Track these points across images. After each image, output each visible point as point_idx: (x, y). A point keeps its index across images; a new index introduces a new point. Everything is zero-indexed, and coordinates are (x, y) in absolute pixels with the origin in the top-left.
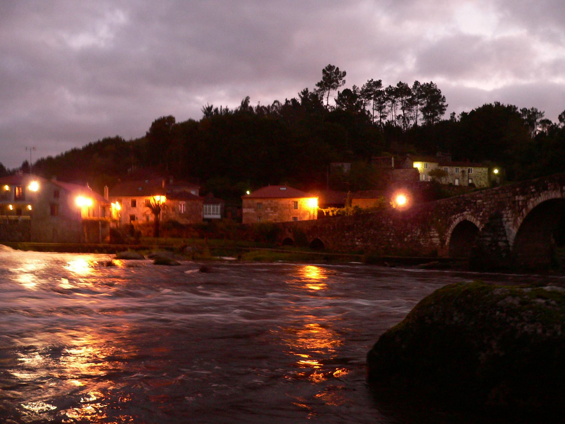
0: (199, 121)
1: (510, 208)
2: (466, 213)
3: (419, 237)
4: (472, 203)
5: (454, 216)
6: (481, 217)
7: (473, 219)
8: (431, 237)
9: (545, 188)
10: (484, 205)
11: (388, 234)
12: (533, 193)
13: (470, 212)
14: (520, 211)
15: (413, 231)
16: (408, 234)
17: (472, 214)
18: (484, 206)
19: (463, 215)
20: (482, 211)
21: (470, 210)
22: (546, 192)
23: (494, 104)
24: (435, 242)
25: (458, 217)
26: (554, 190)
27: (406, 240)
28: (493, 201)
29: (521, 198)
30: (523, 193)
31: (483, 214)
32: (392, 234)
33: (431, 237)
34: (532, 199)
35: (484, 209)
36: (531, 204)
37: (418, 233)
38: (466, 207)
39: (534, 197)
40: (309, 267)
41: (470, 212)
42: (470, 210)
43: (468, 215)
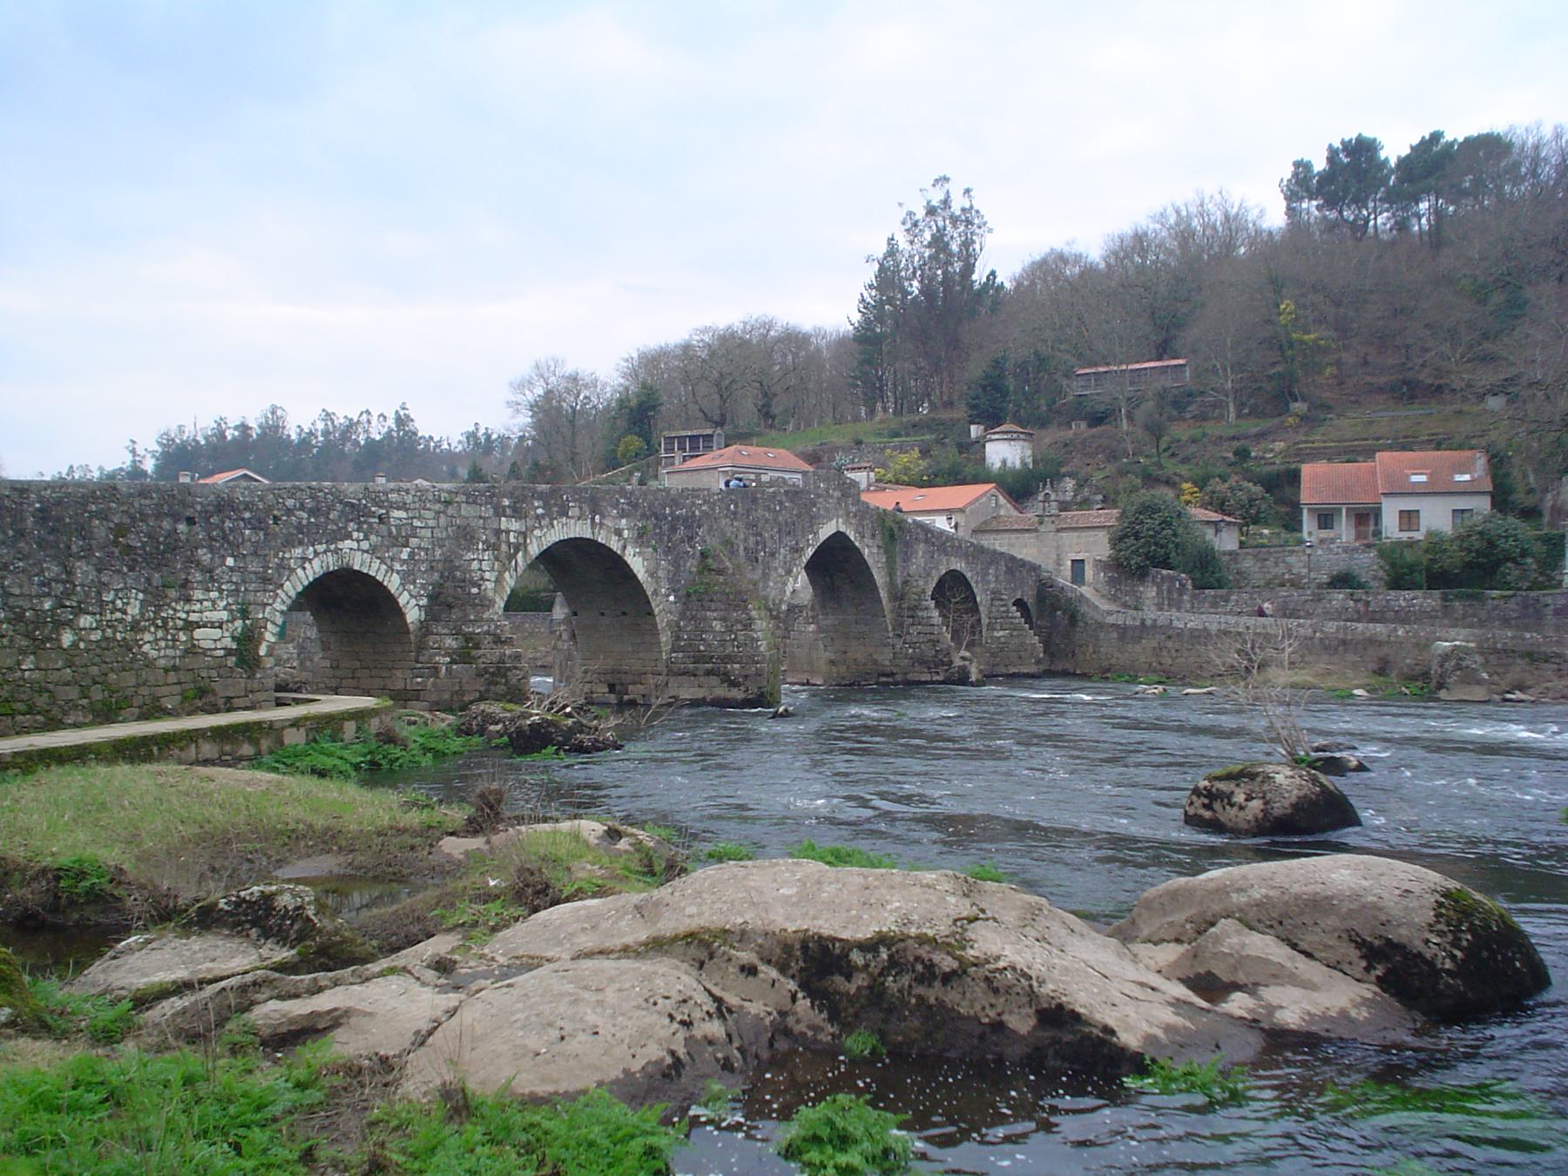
0: (1270, 212)
1: (489, 546)
2: (348, 543)
3: (135, 627)
4: (372, 515)
5: (298, 551)
8: (190, 626)
9: (564, 512)
12: (538, 517)
13: (365, 545)
14: (512, 557)
15: (108, 597)
16: (79, 611)
19: (337, 551)
21: (366, 538)
23: (998, 465)
24: (205, 644)
27: (67, 638)
28: (443, 520)
29: (515, 525)
30: (517, 513)
31: (412, 555)
33: (190, 626)
34: (537, 532)
35: (414, 541)
37: (134, 610)
38: (352, 526)
39: (541, 528)
41: (365, 545)
42: (366, 538)
43: (357, 554)
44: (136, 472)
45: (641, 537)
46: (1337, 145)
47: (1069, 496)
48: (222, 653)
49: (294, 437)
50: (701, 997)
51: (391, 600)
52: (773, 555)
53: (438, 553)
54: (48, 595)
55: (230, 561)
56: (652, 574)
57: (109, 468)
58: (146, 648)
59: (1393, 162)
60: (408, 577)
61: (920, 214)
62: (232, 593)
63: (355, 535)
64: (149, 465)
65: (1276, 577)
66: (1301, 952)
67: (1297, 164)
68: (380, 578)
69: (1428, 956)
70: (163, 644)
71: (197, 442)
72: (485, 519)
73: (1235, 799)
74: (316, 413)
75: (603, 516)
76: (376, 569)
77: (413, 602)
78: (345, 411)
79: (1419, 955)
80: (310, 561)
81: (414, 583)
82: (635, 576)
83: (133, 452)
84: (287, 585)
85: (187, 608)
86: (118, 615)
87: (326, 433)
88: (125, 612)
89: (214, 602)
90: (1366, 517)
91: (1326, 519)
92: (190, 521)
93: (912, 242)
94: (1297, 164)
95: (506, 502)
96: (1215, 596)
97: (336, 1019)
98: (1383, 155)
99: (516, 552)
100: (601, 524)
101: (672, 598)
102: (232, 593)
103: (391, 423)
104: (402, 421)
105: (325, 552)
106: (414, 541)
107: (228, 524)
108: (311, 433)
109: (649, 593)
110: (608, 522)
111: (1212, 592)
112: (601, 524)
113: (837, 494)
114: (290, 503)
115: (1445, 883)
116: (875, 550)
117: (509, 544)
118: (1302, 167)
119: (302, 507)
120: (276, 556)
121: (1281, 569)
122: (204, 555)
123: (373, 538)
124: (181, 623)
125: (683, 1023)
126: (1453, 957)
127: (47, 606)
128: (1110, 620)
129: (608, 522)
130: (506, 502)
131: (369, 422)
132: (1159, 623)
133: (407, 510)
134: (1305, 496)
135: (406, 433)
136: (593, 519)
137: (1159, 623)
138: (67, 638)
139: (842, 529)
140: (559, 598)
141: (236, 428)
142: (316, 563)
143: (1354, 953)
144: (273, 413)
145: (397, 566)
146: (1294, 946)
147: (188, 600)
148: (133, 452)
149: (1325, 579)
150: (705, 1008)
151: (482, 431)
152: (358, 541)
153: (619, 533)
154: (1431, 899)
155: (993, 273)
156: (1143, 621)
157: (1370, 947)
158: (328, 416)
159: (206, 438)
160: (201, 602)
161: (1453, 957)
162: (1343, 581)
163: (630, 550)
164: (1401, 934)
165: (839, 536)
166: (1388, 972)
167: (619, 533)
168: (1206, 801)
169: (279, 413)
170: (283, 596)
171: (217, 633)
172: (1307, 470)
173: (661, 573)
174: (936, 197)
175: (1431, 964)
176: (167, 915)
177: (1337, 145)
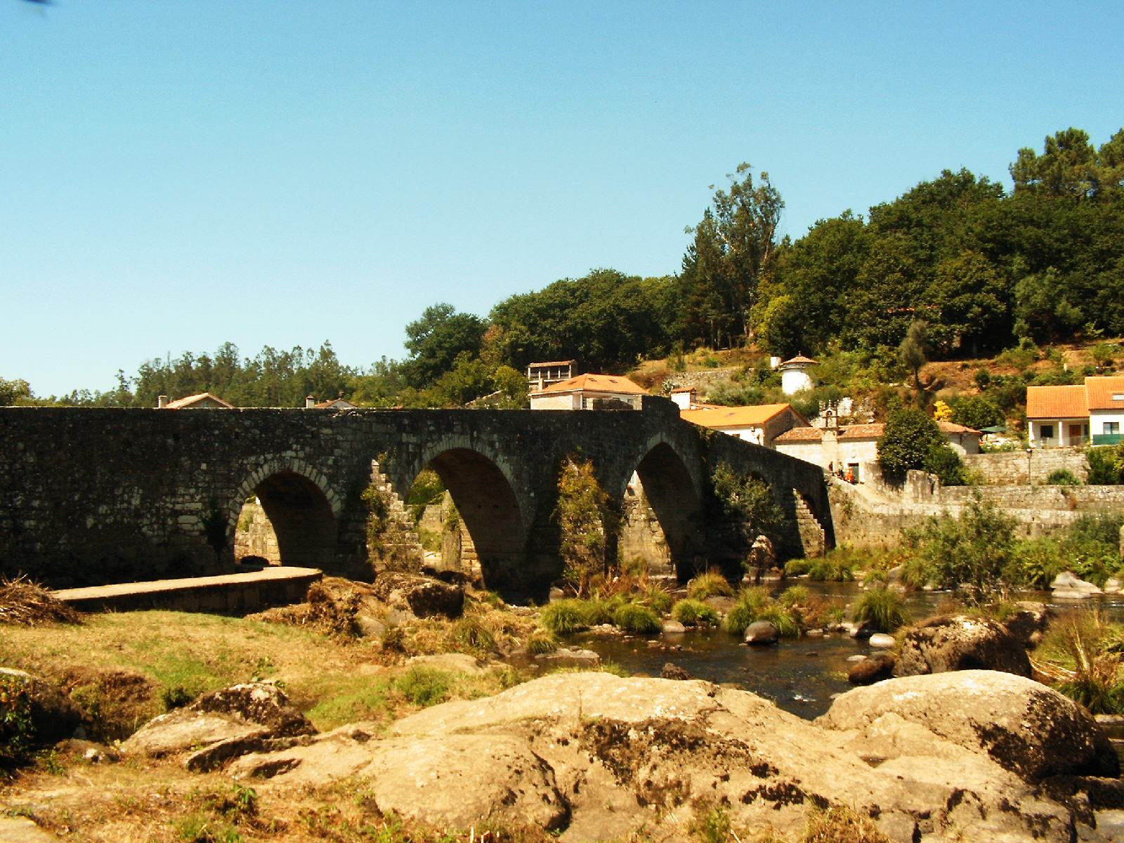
2: (289, 454)
4: (307, 431)
6: (330, 467)
7: (309, 469)
8: (176, 514)
10: (337, 442)
11: (19, 501)
12: (431, 433)
13: (301, 454)
15: (119, 492)
16: (99, 502)
17: (308, 459)
18: (337, 444)
19: (281, 459)
20: (332, 454)
21: (302, 449)
22: (450, 435)
25: (266, 461)
26: (461, 434)
27: (90, 522)
29: (413, 439)
31: (335, 461)
32: (36, 503)
34: (430, 445)
36: (428, 452)
37: (136, 502)
38: (291, 440)
39: (432, 441)
40: (236, 555)
41: (301, 454)
42: (302, 449)
43: (295, 460)
44: (124, 394)
45: (507, 450)
46: (1053, 136)
47: (848, 412)
48: (197, 533)
49: (243, 367)
50: (528, 755)
51: (321, 495)
52: (611, 461)
53: (356, 459)
54: (77, 490)
55: (204, 466)
56: (517, 476)
57: (103, 392)
58: (144, 529)
59: (1097, 150)
60: (332, 479)
61: (728, 193)
62: (206, 490)
63: (294, 446)
64: (133, 389)
65: (1006, 476)
66: (939, 734)
67: (1022, 153)
68: (312, 479)
69: (1021, 735)
70: (156, 526)
71: (170, 372)
72: (390, 434)
73: (934, 641)
74: (259, 349)
75: (479, 432)
76: (309, 472)
77: (337, 497)
78: (283, 346)
79: (1016, 735)
80: (262, 466)
81: (337, 483)
82: (505, 478)
83: (122, 379)
84: (245, 484)
85: (173, 500)
86: (125, 505)
87: (267, 364)
88: (130, 503)
89: (192, 496)
90: (1078, 429)
91: (1046, 432)
92: (176, 438)
93: (722, 215)
94: (1022, 153)
95: (406, 422)
96: (957, 491)
97: (290, 765)
98: (1089, 143)
99: (414, 460)
100: (478, 438)
101: (532, 495)
102: (206, 490)
103: (317, 356)
104: (327, 354)
105: (273, 459)
106: (337, 452)
107: (203, 439)
108: (256, 364)
109: (515, 491)
110: (484, 437)
111: (955, 488)
112: (478, 438)
113: (661, 413)
114: (247, 423)
115: (1038, 688)
116: (691, 457)
117: (408, 453)
118: (1026, 155)
119: (256, 426)
120: (237, 462)
121: (1011, 469)
122: (185, 462)
123: (307, 449)
124: (168, 511)
125: (517, 772)
126: (1039, 737)
127: (76, 498)
128: (877, 510)
129: (484, 437)
130: (406, 422)
131: (300, 355)
132: (914, 513)
133: (332, 428)
134: (1031, 411)
135: (329, 364)
136: (472, 433)
137: (914, 513)
138: (90, 522)
139: (665, 440)
140: (447, 495)
141: (199, 360)
142: (266, 467)
143: (974, 736)
144: (228, 348)
145: (325, 470)
146: (935, 731)
147: (174, 494)
148: (122, 379)
149: (1044, 478)
150: (531, 763)
151: (388, 362)
152: (296, 451)
153: (492, 444)
154: (1027, 698)
155: (787, 238)
156: (902, 511)
157: (984, 730)
158: (270, 351)
159: (176, 367)
160: (183, 496)
161: (1039, 737)
162: (1058, 478)
163: (500, 458)
164: (1003, 722)
165: (663, 446)
166: (996, 747)
167: (492, 444)
168: (915, 643)
169: (232, 348)
170: (242, 492)
171: (193, 519)
172: (1032, 391)
173: (524, 475)
174: (741, 180)
175: (1023, 741)
176: (178, 701)
177: (1053, 136)
